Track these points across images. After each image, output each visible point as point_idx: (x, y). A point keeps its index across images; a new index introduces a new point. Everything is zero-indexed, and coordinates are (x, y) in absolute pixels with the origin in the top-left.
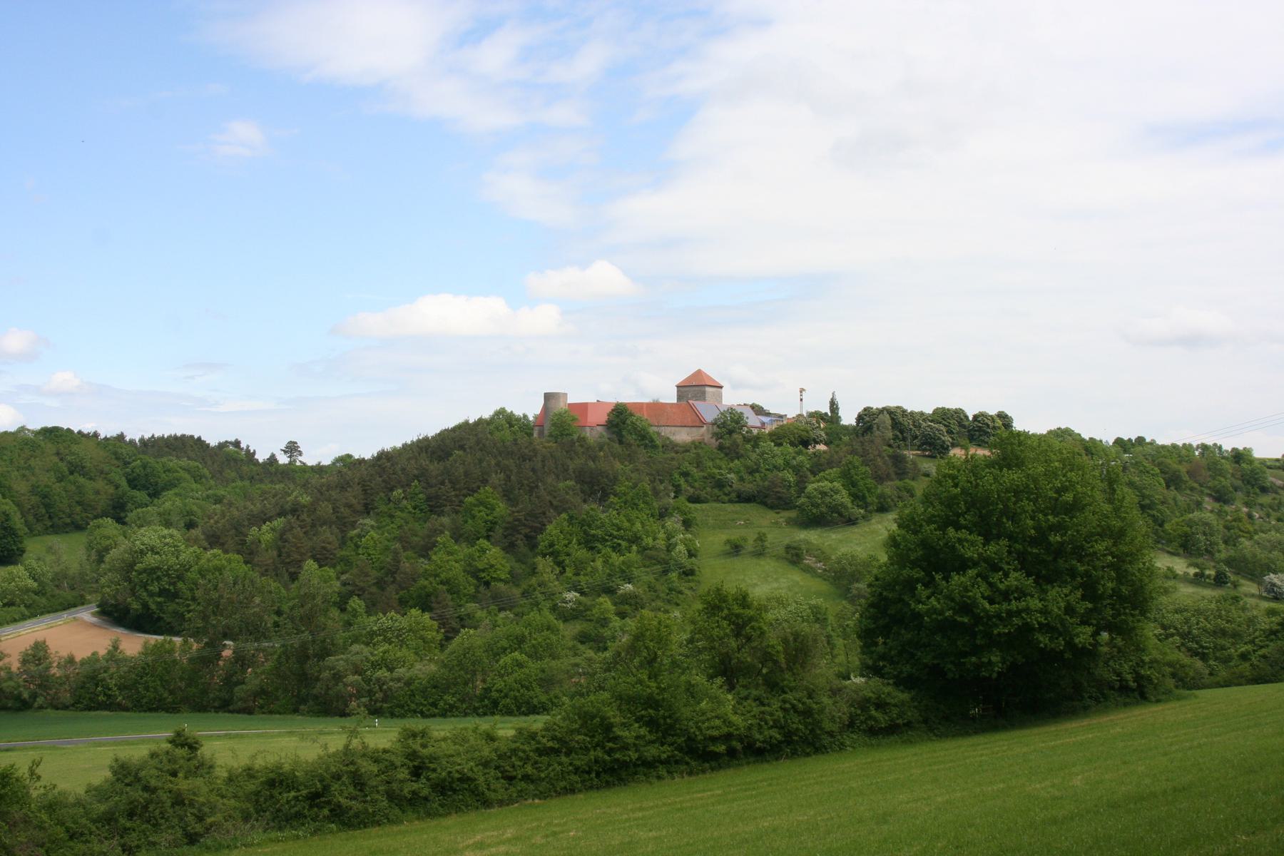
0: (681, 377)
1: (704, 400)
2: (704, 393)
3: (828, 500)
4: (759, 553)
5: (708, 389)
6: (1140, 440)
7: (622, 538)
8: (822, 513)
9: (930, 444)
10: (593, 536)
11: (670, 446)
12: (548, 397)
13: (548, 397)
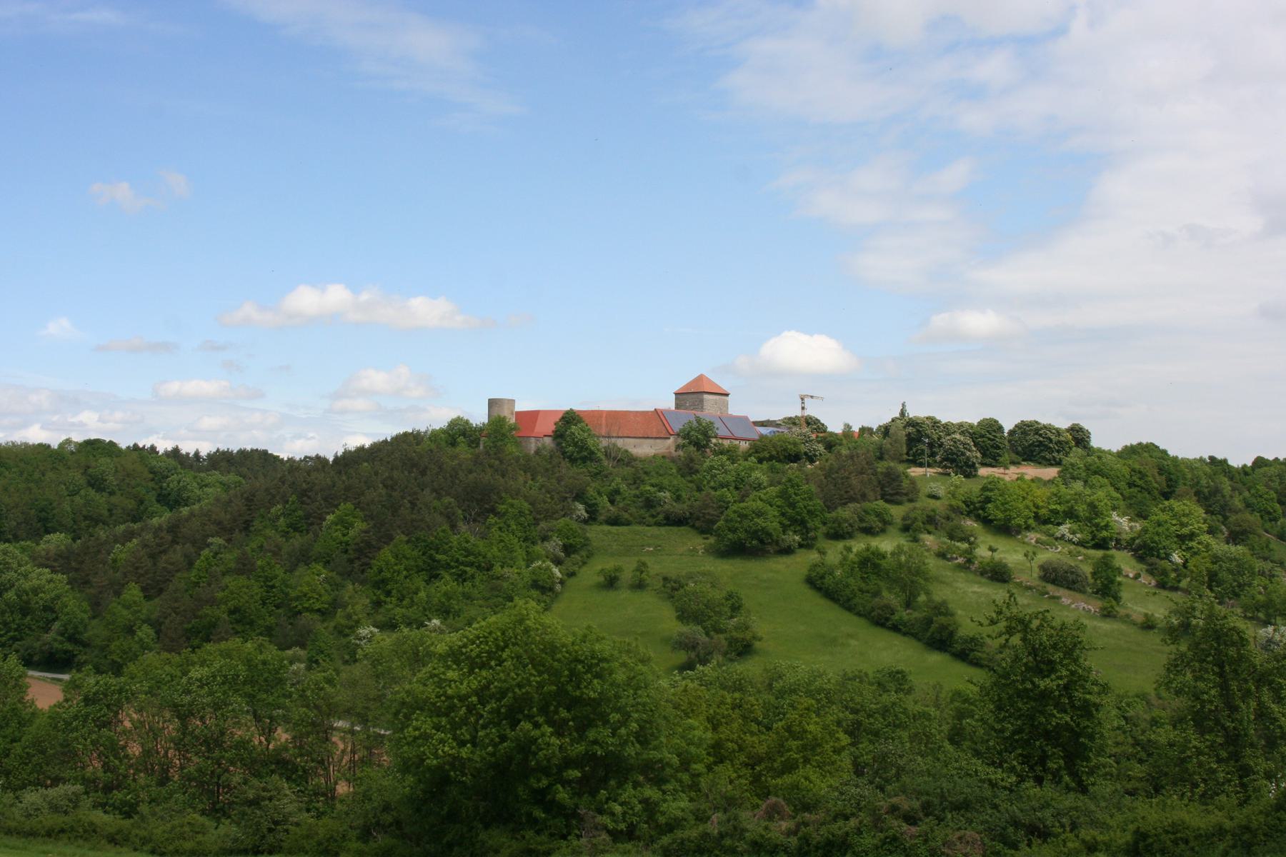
0: (679, 384)
1: (513, 401)
2: (702, 401)
3: (746, 523)
4: (639, 586)
5: (706, 396)
6: (1260, 462)
7: (471, 564)
8: (740, 539)
9: (953, 461)
10: (438, 561)
11: (626, 460)
12: (492, 403)
13: (492, 403)
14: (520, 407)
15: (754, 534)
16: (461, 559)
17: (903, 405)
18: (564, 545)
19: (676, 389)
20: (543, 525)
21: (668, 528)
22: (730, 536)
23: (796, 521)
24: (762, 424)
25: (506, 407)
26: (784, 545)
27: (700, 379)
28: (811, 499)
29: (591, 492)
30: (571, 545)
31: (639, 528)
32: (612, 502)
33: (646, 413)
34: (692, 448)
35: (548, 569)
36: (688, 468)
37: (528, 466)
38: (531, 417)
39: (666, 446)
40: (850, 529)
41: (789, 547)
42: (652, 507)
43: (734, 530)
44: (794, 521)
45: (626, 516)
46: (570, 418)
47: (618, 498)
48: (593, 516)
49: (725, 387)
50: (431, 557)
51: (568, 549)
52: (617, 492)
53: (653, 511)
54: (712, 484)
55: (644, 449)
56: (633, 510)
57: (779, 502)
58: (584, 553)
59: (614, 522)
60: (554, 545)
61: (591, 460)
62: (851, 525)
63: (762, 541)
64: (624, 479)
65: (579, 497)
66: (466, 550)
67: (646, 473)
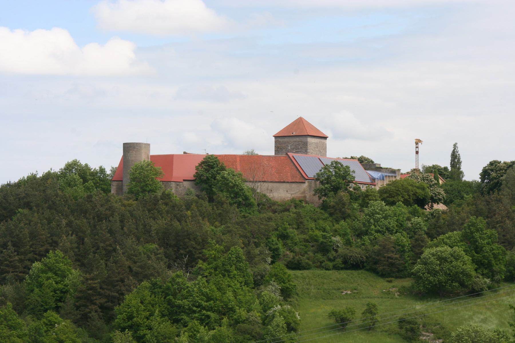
2: (306, 144)
3: (446, 266)
4: (369, 328)
5: (310, 140)
7: (210, 309)
8: (440, 282)
10: (179, 306)
11: (267, 205)
12: (128, 148)
14: (154, 152)
17: (455, 146)
19: (276, 131)
21: (349, 272)
25: (143, 151)
27: (300, 122)
31: (319, 272)
38: (167, 160)
43: (435, 273)
49: (325, 132)
50: (169, 303)
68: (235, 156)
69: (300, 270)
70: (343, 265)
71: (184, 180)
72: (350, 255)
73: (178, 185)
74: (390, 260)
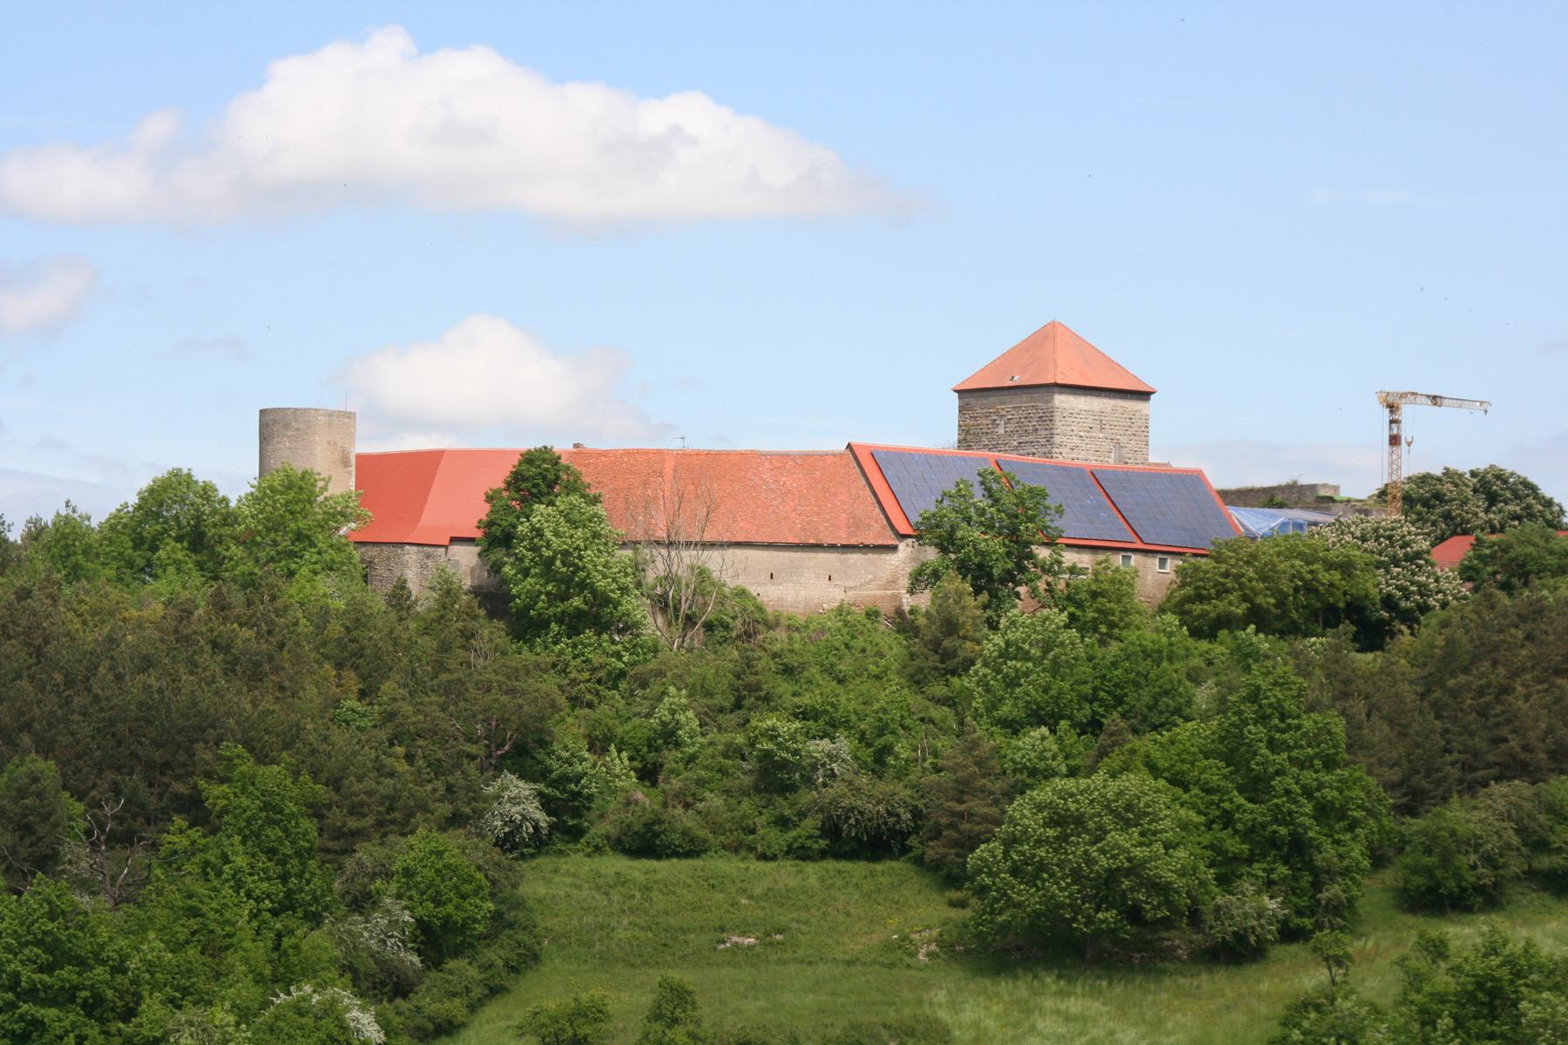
0: (974, 360)
2: (1047, 418)
5: (1061, 401)
7: (64, 997)
11: (734, 626)
12: (272, 425)
15: (1106, 887)
16: (27, 975)
18: (422, 925)
19: (967, 371)
20: (367, 854)
21: (831, 865)
22: (1021, 892)
23: (1274, 842)
24: (1269, 498)
26: (1221, 931)
27: (1048, 336)
28: (1330, 764)
29: (569, 735)
30: (448, 925)
31: (724, 865)
32: (649, 774)
33: (808, 461)
34: (956, 584)
35: (331, 1009)
36: (936, 650)
37: (357, 653)
38: (400, 478)
39: (885, 578)
40: (1487, 876)
41: (1240, 937)
42: (787, 788)
44: (1263, 844)
45: (685, 820)
46: (538, 477)
47: (671, 757)
48: (568, 814)
49: (1148, 380)
51: (436, 941)
52: (669, 735)
53: (784, 808)
54: (1005, 710)
55: (802, 589)
56: (714, 801)
57: (1214, 772)
58: (494, 955)
59: (645, 843)
60: (385, 930)
61: (602, 626)
62: (1489, 860)
63: (1134, 914)
64: (700, 690)
65: (523, 752)
66: (51, 945)
67: (788, 671)
68: (822, 456)
69: (659, 857)
70: (823, 843)
71: (454, 540)
72: (845, 803)
73: (428, 557)
74: (965, 826)
